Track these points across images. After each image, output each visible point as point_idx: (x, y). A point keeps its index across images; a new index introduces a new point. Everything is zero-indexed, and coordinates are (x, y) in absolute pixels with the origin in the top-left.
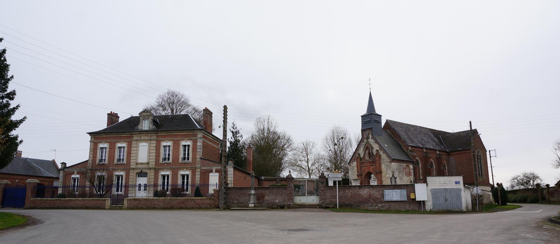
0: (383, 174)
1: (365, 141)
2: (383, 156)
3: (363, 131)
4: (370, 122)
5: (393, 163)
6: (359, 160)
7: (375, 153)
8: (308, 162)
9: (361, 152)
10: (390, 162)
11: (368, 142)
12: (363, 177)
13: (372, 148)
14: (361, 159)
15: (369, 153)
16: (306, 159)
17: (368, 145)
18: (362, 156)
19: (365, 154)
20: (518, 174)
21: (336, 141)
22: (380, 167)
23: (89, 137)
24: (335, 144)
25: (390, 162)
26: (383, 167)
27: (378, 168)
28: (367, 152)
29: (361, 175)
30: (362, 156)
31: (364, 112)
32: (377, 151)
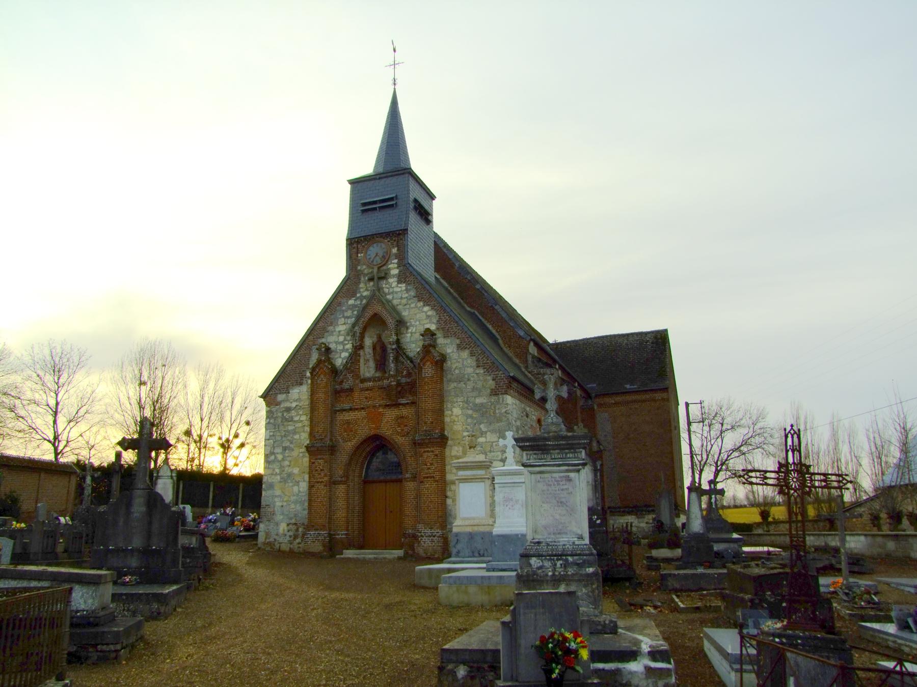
0: (453, 451)
1: (365, 289)
2: (460, 360)
3: (355, 244)
4: (388, 204)
5: (509, 399)
6: (323, 380)
7: (413, 343)
8: (56, 413)
9: (340, 344)
10: (494, 393)
11: (377, 296)
12: (343, 457)
13: (401, 324)
14: (334, 371)
15: (380, 350)
16: (52, 402)
17: (378, 308)
18: (340, 359)
19: (358, 348)
20: (438, 211)
21: (145, 378)
22: (440, 412)
23: (349, 186)
24: (142, 383)
25: (494, 393)
26: (457, 416)
27: (429, 418)
28: (368, 342)
29: (333, 449)
30: (340, 359)
31: (366, 166)
32: (428, 333)
